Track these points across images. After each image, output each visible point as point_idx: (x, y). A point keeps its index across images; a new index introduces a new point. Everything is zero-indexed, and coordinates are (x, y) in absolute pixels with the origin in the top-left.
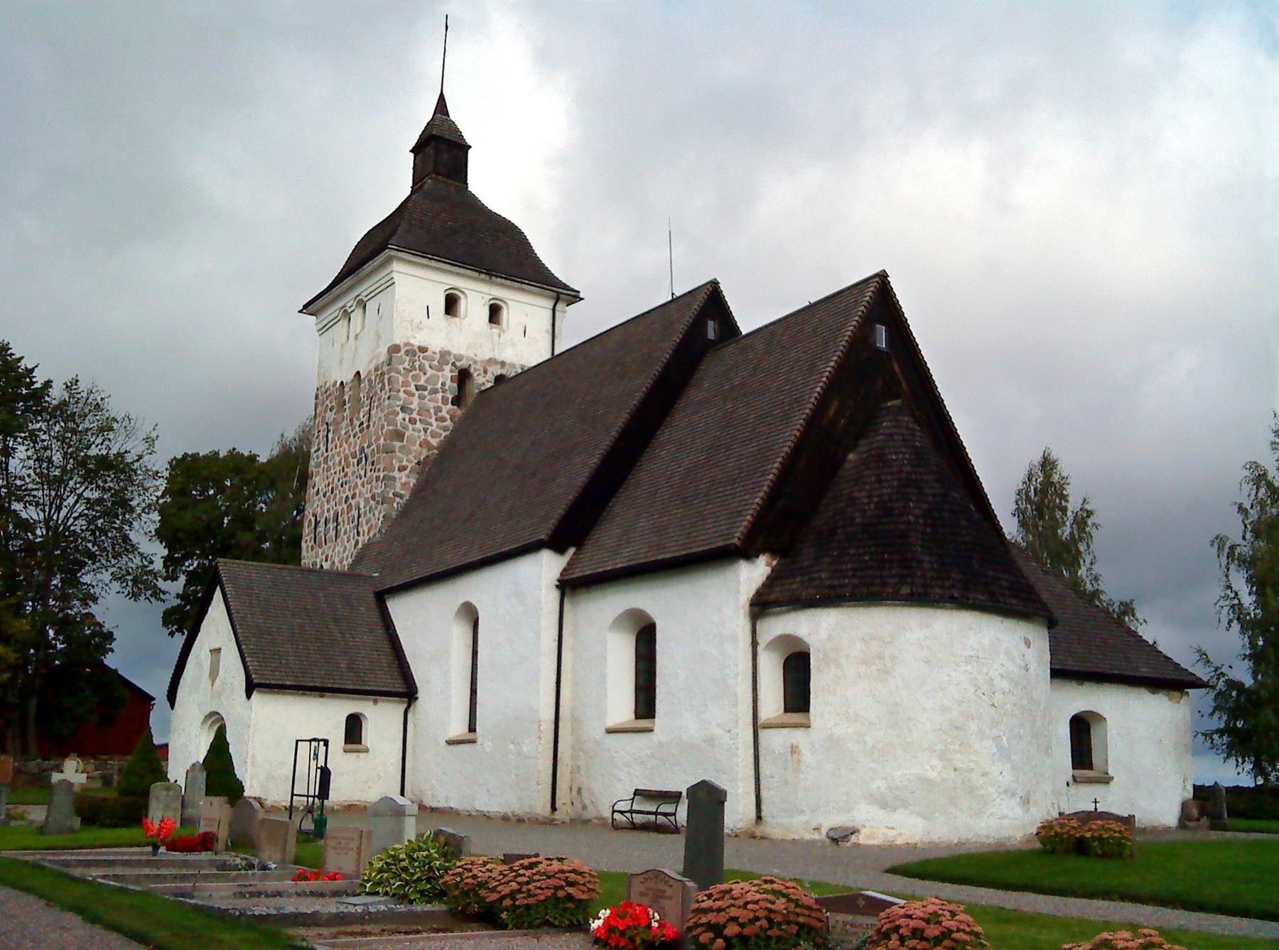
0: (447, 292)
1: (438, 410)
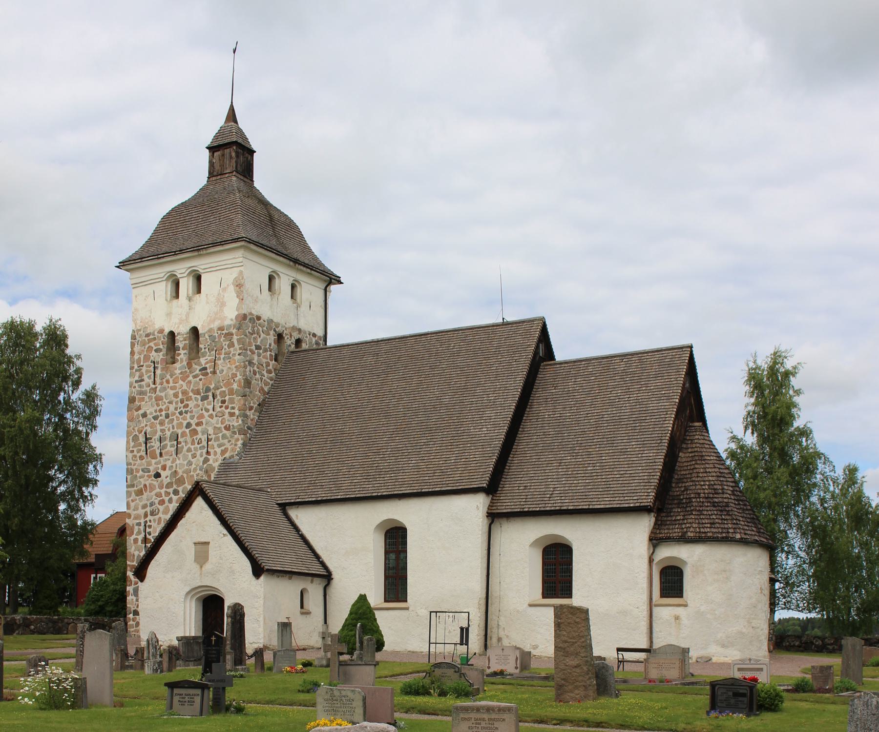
0: (294, 282)
1: (268, 365)
